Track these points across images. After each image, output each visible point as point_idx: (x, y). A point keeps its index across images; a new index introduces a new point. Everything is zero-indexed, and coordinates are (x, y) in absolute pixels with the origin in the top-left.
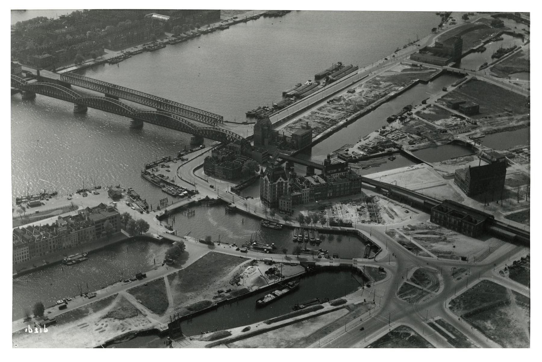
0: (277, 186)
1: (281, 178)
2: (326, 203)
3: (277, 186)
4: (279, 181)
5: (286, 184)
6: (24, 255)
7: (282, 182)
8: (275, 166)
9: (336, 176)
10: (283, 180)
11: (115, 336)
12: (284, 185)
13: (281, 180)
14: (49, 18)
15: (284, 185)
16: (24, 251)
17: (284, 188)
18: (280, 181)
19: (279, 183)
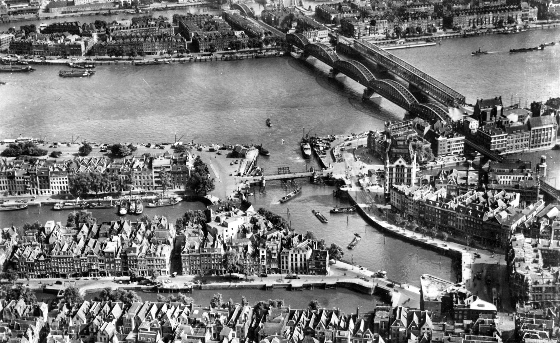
0: (394, 170)
1: (400, 159)
2: (490, 222)
3: (394, 170)
4: (397, 163)
5: (409, 170)
6: (62, 185)
7: (403, 166)
8: (91, 302)
9: (508, 180)
10: (404, 163)
11: (526, 54)
12: (406, 170)
13: (400, 162)
14: (273, 212)
15: (406, 170)
16: (62, 181)
17: (406, 176)
18: (400, 165)
19: (398, 166)
